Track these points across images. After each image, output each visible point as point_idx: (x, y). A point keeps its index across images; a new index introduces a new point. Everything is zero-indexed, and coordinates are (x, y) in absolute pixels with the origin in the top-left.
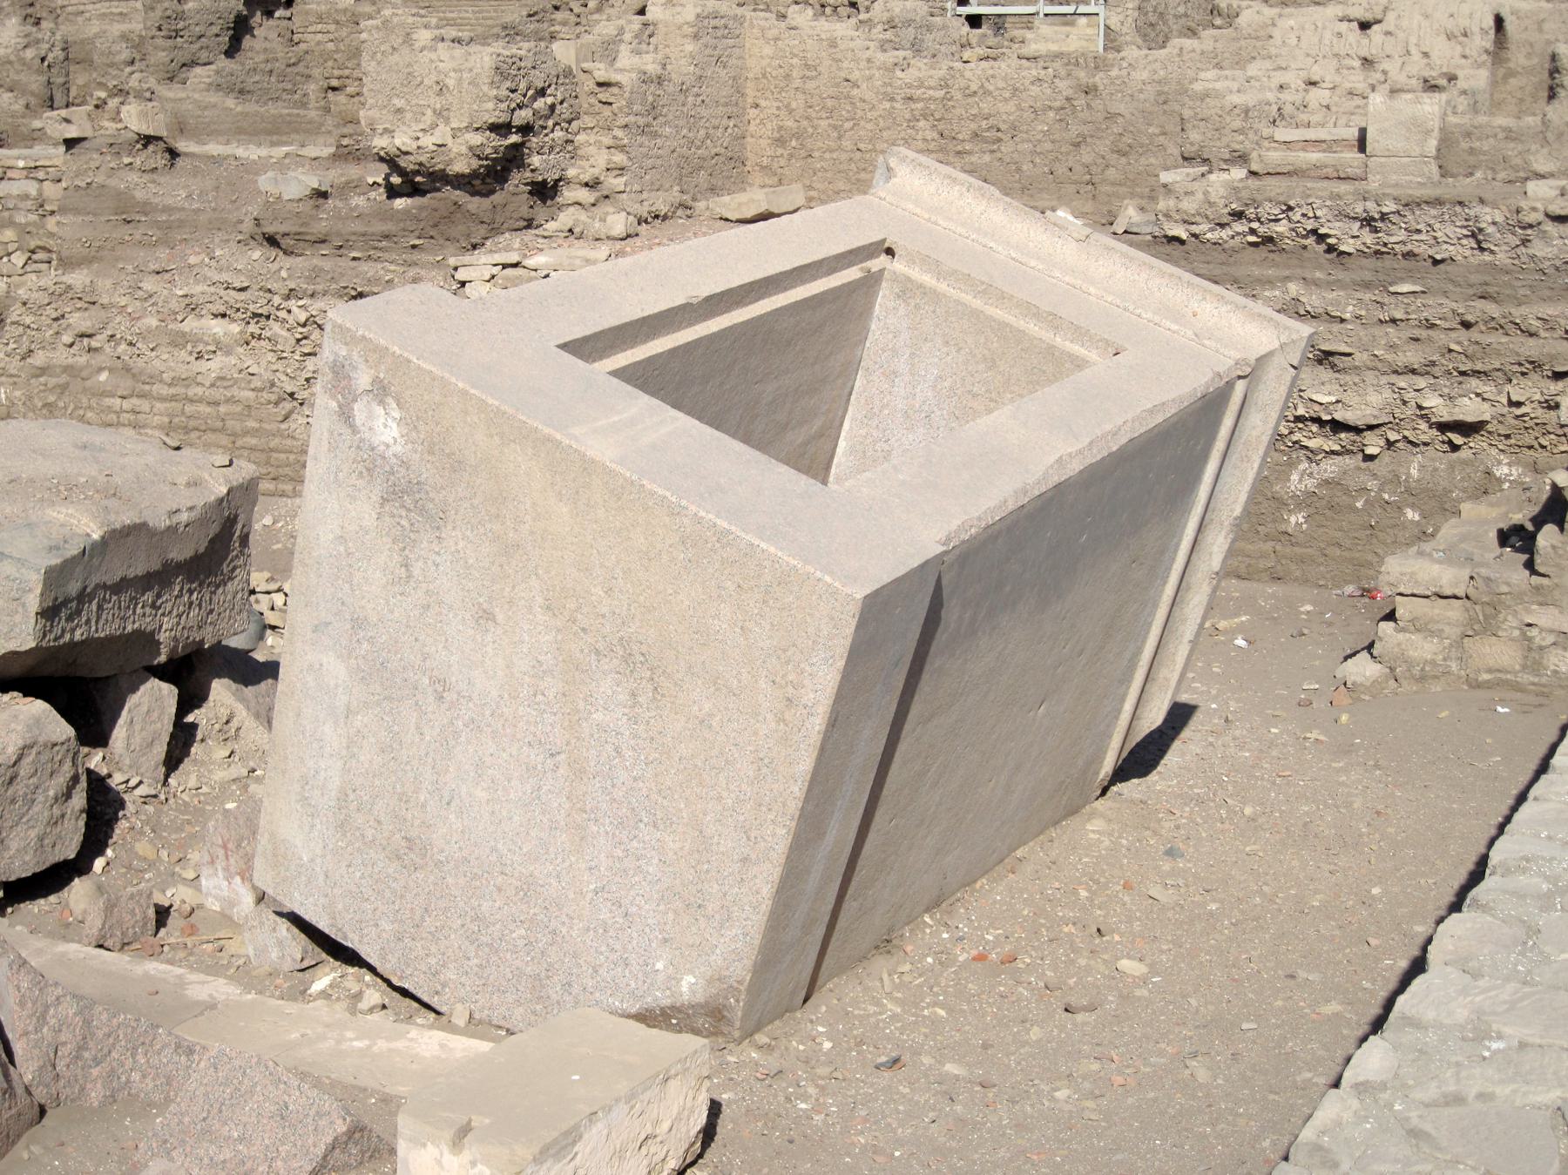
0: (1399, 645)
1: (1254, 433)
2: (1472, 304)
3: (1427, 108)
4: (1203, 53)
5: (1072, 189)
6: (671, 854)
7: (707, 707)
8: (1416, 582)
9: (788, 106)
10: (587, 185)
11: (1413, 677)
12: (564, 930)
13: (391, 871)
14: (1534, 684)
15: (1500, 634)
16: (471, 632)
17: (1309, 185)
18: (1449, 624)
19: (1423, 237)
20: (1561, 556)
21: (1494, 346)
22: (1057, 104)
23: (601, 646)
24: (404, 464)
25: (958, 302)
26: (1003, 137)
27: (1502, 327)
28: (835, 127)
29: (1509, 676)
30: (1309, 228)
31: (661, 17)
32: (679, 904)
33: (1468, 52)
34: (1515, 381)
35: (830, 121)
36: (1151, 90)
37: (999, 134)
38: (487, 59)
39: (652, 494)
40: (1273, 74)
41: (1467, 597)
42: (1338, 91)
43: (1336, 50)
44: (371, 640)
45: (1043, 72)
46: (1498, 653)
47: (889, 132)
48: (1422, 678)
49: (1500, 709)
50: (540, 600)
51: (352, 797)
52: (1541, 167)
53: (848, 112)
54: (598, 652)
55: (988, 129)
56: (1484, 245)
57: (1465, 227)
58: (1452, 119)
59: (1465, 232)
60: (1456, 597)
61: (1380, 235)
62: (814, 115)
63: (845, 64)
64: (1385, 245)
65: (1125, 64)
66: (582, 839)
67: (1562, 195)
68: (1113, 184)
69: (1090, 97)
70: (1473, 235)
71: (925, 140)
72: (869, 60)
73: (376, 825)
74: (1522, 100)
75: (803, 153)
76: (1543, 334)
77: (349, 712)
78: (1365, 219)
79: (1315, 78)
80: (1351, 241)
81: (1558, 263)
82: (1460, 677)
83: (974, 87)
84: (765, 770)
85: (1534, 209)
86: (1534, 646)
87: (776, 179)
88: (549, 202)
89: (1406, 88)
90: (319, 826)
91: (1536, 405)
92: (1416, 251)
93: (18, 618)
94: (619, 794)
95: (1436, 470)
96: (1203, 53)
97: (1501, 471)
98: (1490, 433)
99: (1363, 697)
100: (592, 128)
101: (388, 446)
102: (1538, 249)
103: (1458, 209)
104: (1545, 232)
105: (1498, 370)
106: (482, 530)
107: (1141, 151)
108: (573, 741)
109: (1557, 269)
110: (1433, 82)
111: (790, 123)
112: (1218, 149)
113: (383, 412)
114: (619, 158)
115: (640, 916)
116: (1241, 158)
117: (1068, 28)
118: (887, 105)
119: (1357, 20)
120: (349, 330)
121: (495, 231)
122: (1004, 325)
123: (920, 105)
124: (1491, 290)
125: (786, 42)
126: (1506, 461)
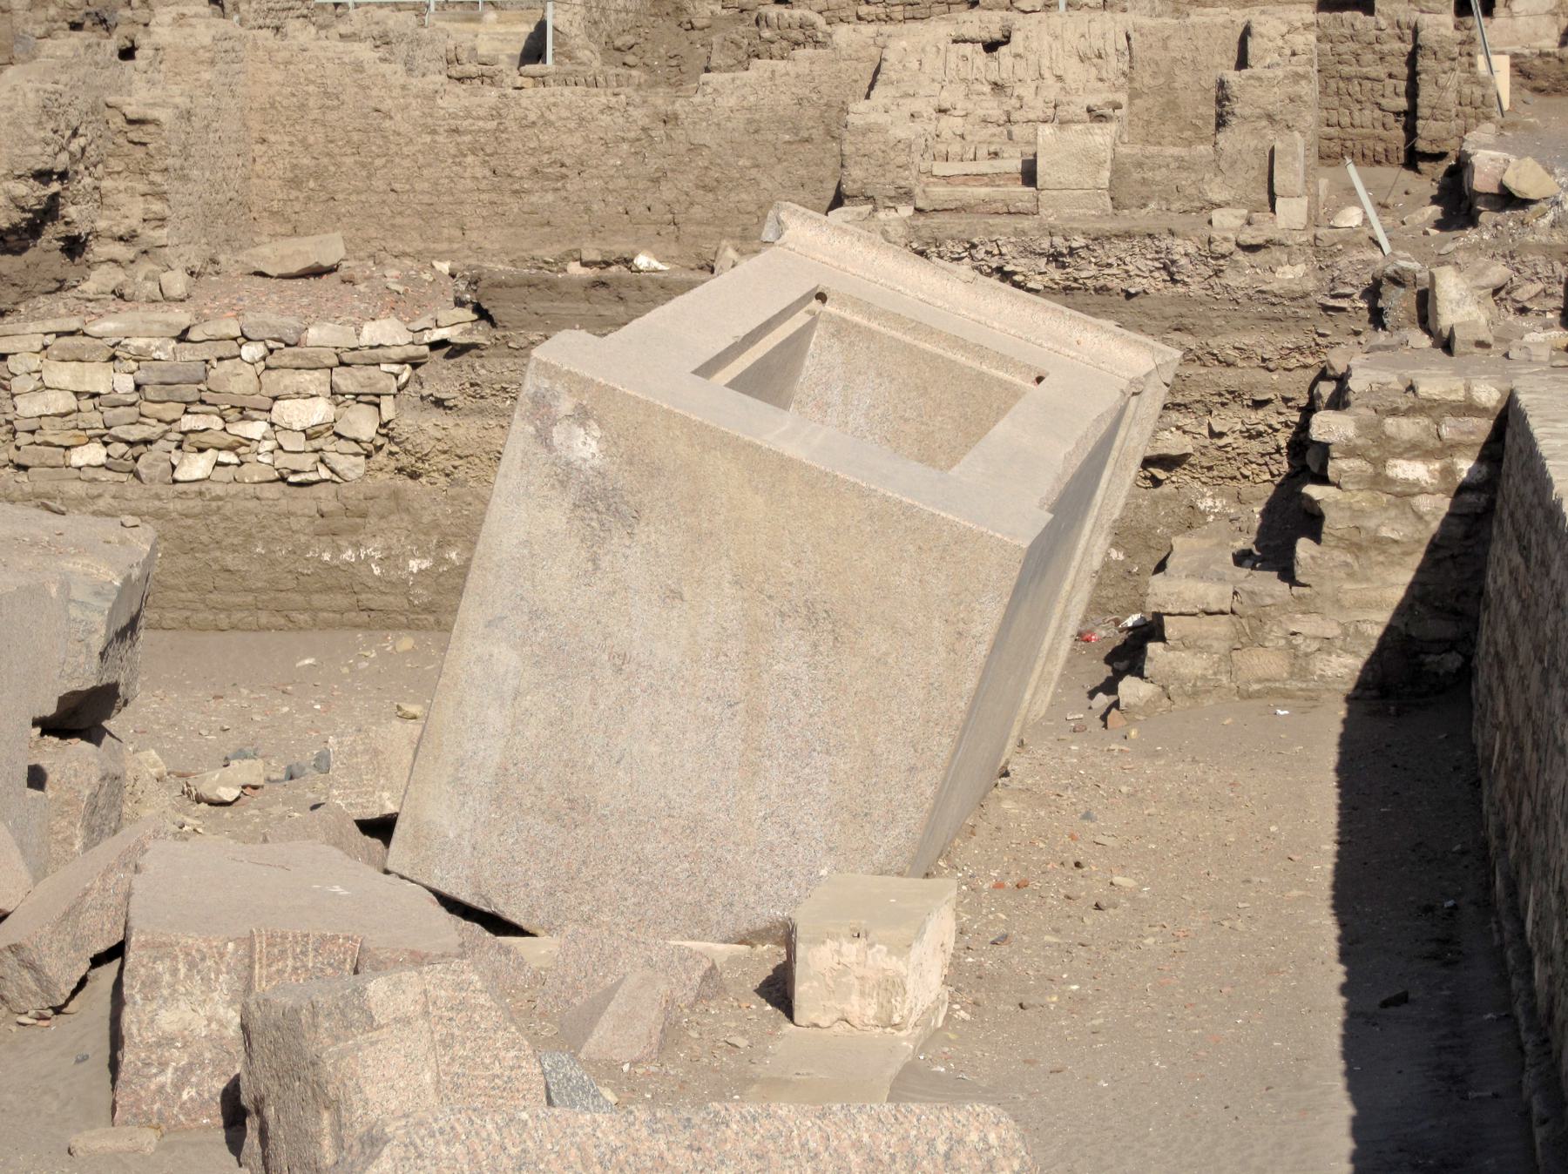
0: (1170, 663)
1: (1132, 444)
2: (1169, 336)
3: (1099, 139)
4: (798, 76)
5: (651, 230)
6: (841, 774)
7: (883, 648)
8: (1184, 600)
9: (303, 141)
10: (121, 239)
11: (1185, 693)
12: (729, 857)
13: (548, 832)
14: (1301, 690)
15: (1267, 644)
16: (656, 610)
17: (991, 221)
18: (1217, 639)
19: (1114, 271)
20: (1320, 565)
21: (1194, 377)
22: (632, 135)
23: (785, 609)
24: (601, 474)
25: (892, 338)
26: (568, 173)
27: (1199, 358)
28: (363, 165)
29: (1277, 685)
30: (994, 266)
31: (169, 39)
32: (846, 816)
33: (1104, 75)
34: (1215, 412)
35: (357, 157)
36: (741, 118)
37: (564, 170)
38: (31, 95)
39: (845, 482)
40: (901, 101)
41: (1233, 612)
42: (970, 119)
43: (963, 75)
44: (549, 628)
45: (614, 100)
46: (1265, 663)
47: (432, 170)
48: (1195, 694)
49: (1280, 712)
50: (729, 577)
51: (512, 771)
52: (1216, 197)
53: (380, 147)
54: (782, 614)
55: (550, 165)
56: (1177, 277)
57: (1157, 260)
58: (1123, 150)
59: (1157, 264)
60: (1222, 613)
61: (1068, 270)
62: (336, 151)
63: (375, 92)
64: (1076, 280)
65: (709, 90)
66: (754, 774)
67: (1249, 223)
68: (699, 223)
69: (669, 126)
70: (1165, 268)
71: (475, 178)
72: (404, 87)
73: (537, 792)
74: (1149, 122)
75: (323, 196)
76: (1240, 363)
77: (517, 694)
78: (1052, 255)
79: (946, 105)
80: (1039, 278)
81: (1251, 292)
82: (1230, 690)
83: (532, 117)
84: (935, 693)
85: (1226, 239)
86: (1300, 653)
87: (290, 226)
88: (77, 260)
89: (1076, 118)
90: (471, 803)
91: (1237, 435)
92: (1110, 285)
93: (82, 659)
94: (794, 730)
95: (1139, 506)
96: (798, 76)
97: (1205, 504)
98: (1192, 465)
99: (1137, 717)
100: (119, 173)
101: (585, 460)
102: (1231, 278)
103: (1148, 241)
104: (1237, 262)
105: (1198, 402)
106: (676, 524)
107: (730, 185)
108: (752, 692)
109: (1250, 298)
110: (1099, 112)
111: (306, 161)
112: (883, 186)
113: (582, 432)
114: (157, 207)
115: (807, 832)
116: (906, 195)
117: (473, 25)
118: (428, 139)
119: (983, 42)
120: (553, 366)
121: (28, 294)
122: (935, 357)
123: (468, 138)
124: (1186, 321)
125: (300, 66)
126: (1210, 493)
